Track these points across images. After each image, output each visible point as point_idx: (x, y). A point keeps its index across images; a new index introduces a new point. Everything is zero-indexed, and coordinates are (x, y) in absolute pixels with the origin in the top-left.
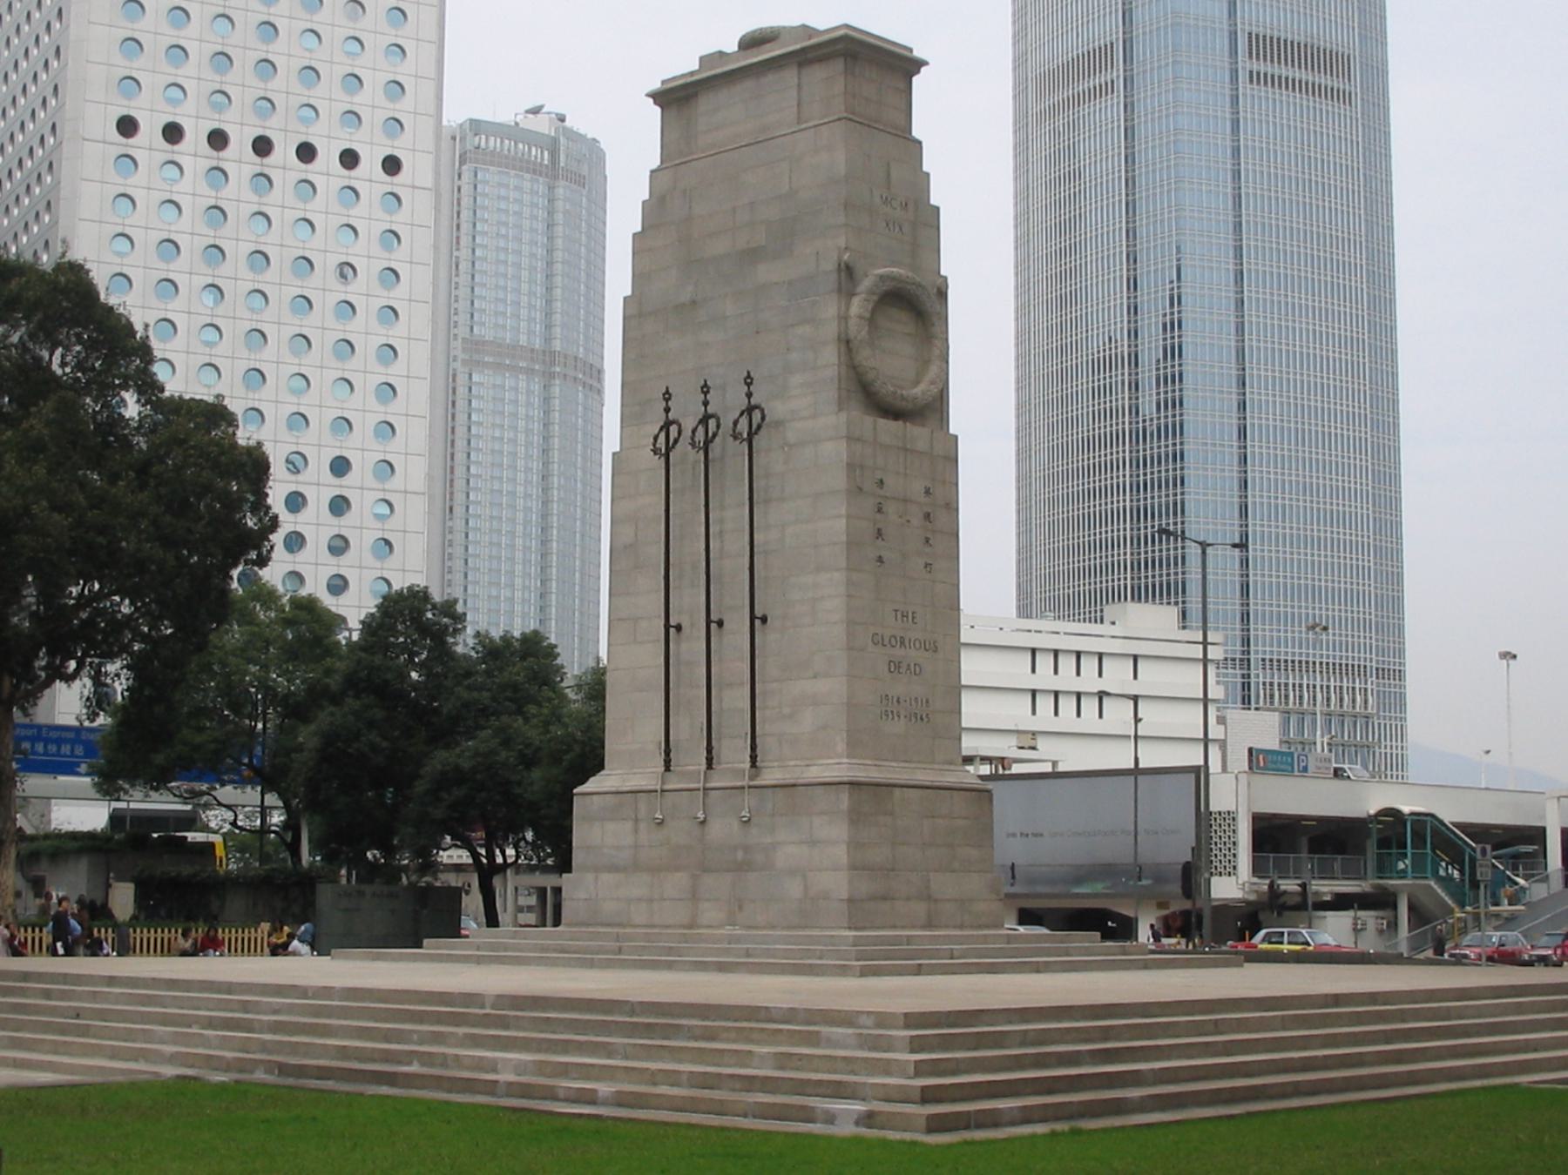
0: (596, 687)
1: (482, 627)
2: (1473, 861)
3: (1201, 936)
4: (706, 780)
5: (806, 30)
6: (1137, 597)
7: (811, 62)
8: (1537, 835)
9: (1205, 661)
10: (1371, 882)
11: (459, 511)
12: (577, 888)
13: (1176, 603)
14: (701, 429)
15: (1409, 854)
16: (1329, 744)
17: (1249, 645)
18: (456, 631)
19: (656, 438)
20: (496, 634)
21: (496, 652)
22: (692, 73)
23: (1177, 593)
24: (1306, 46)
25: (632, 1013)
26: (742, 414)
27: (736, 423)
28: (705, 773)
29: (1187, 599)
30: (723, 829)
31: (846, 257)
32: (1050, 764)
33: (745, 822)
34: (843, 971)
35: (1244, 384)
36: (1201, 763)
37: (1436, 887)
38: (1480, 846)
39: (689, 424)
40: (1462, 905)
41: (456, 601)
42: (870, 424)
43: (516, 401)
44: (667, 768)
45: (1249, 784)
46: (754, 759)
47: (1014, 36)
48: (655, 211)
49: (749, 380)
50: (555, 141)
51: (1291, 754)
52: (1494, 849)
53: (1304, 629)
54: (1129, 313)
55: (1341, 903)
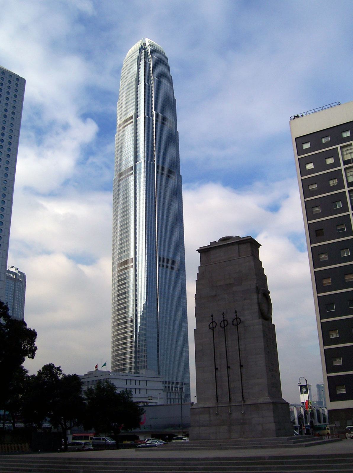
4: (230, 404)
7: (241, 244)
32: (155, 403)
44: (217, 402)
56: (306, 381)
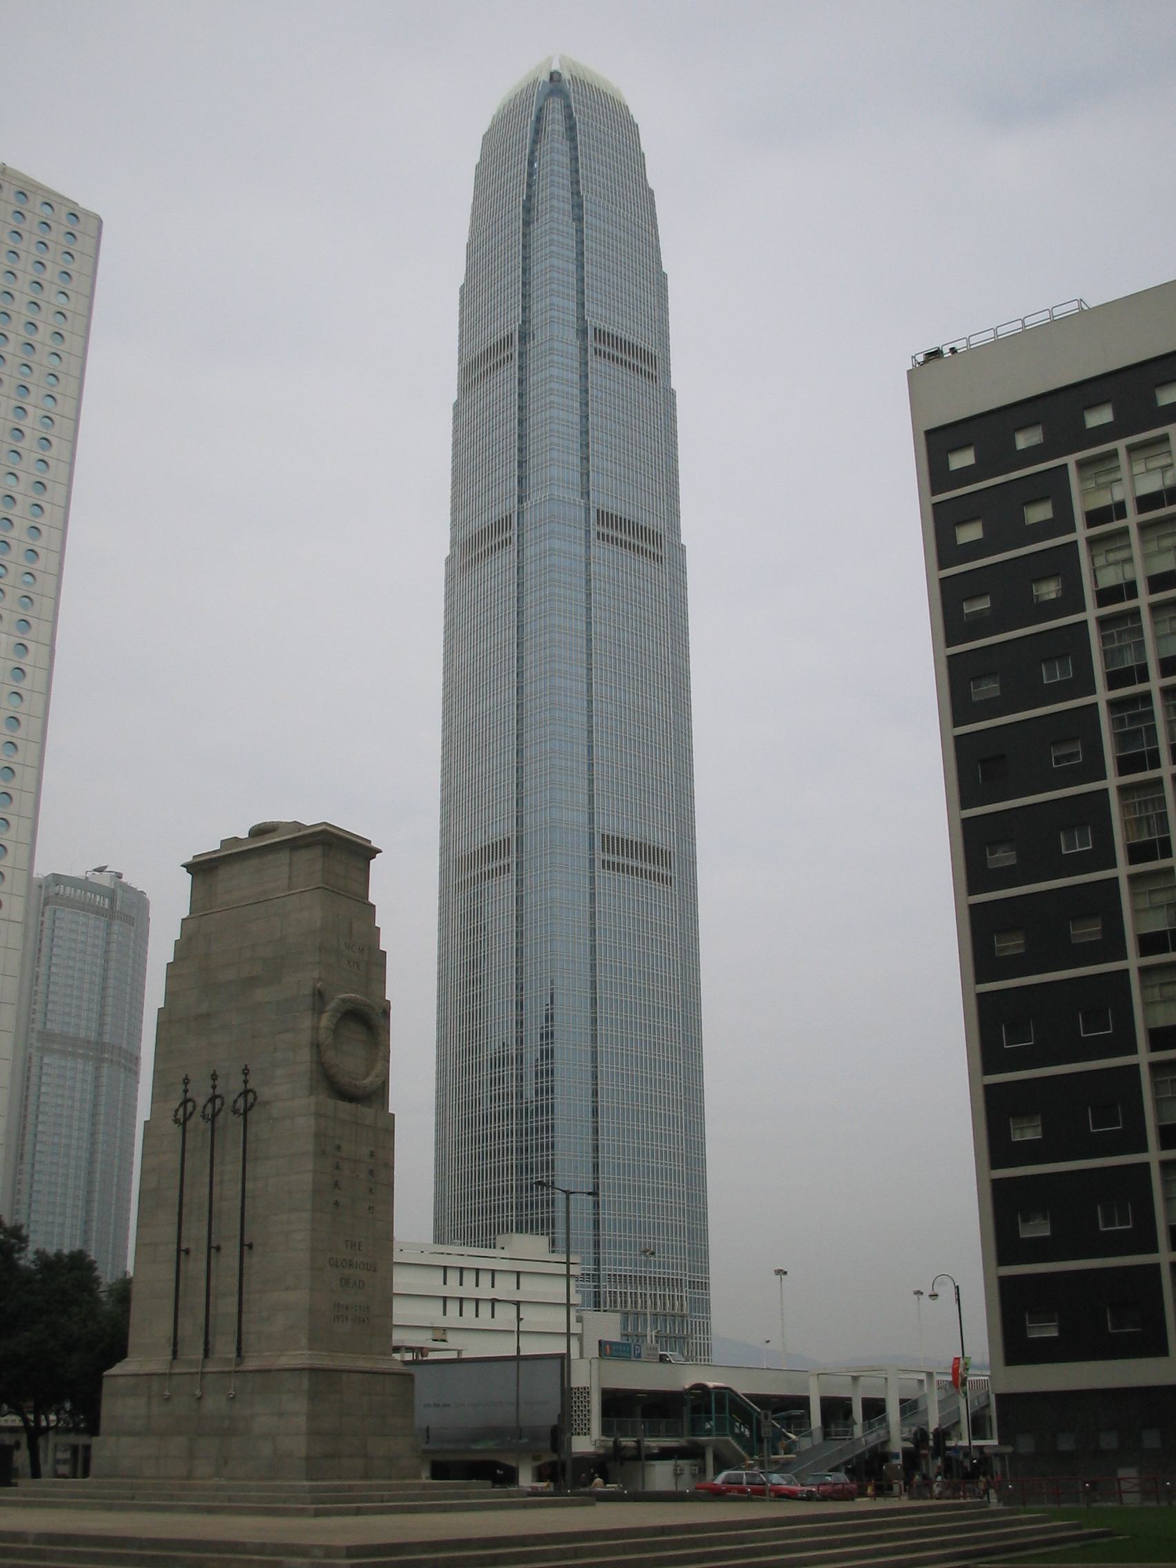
0: (123, 1292)
1: (40, 1246)
2: (759, 1422)
3: (565, 1481)
4: (203, 1367)
5: (297, 825)
6: (519, 1230)
8: (803, 1402)
9: (568, 1276)
10: (686, 1438)
11: (27, 1157)
12: (103, 1448)
13: (548, 1234)
14: (210, 1106)
15: (714, 1418)
16: (656, 1336)
17: (599, 1265)
18: (21, 1250)
19: (177, 1111)
20: (51, 1250)
21: (51, 1265)
22: (215, 852)
23: (548, 1227)
24: (641, 844)
25: (141, 1548)
26: (239, 1096)
27: (235, 1102)
28: (203, 1360)
29: (555, 1096)
30: (214, 1403)
31: (319, 985)
33: (232, 1398)
34: (301, 1513)
35: (597, 1078)
36: (566, 1352)
37: (733, 1442)
38: (764, 1411)
39: (201, 1101)
40: (751, 1455)
41: (21, 1227)
42: (333, 1105)
43: (74, 1078)
45: (599, 1367)
46: (239, 1350)
47: (441, 831)
48: (183, 948)
49: (246, 1072)
50: (113, 891)
51: (629, 1345)
52: (774, 1412)
53: (638, 1253)
54: (517, 1026)
55: (665, 1454)
56: (957, 1288)
